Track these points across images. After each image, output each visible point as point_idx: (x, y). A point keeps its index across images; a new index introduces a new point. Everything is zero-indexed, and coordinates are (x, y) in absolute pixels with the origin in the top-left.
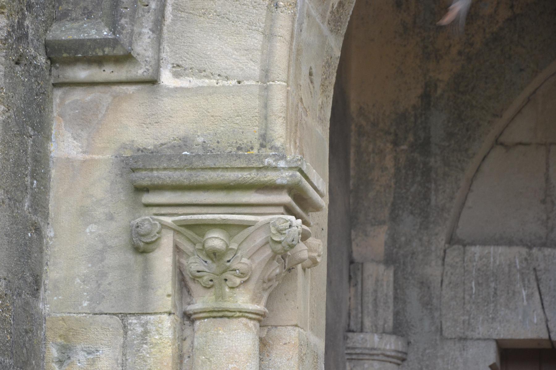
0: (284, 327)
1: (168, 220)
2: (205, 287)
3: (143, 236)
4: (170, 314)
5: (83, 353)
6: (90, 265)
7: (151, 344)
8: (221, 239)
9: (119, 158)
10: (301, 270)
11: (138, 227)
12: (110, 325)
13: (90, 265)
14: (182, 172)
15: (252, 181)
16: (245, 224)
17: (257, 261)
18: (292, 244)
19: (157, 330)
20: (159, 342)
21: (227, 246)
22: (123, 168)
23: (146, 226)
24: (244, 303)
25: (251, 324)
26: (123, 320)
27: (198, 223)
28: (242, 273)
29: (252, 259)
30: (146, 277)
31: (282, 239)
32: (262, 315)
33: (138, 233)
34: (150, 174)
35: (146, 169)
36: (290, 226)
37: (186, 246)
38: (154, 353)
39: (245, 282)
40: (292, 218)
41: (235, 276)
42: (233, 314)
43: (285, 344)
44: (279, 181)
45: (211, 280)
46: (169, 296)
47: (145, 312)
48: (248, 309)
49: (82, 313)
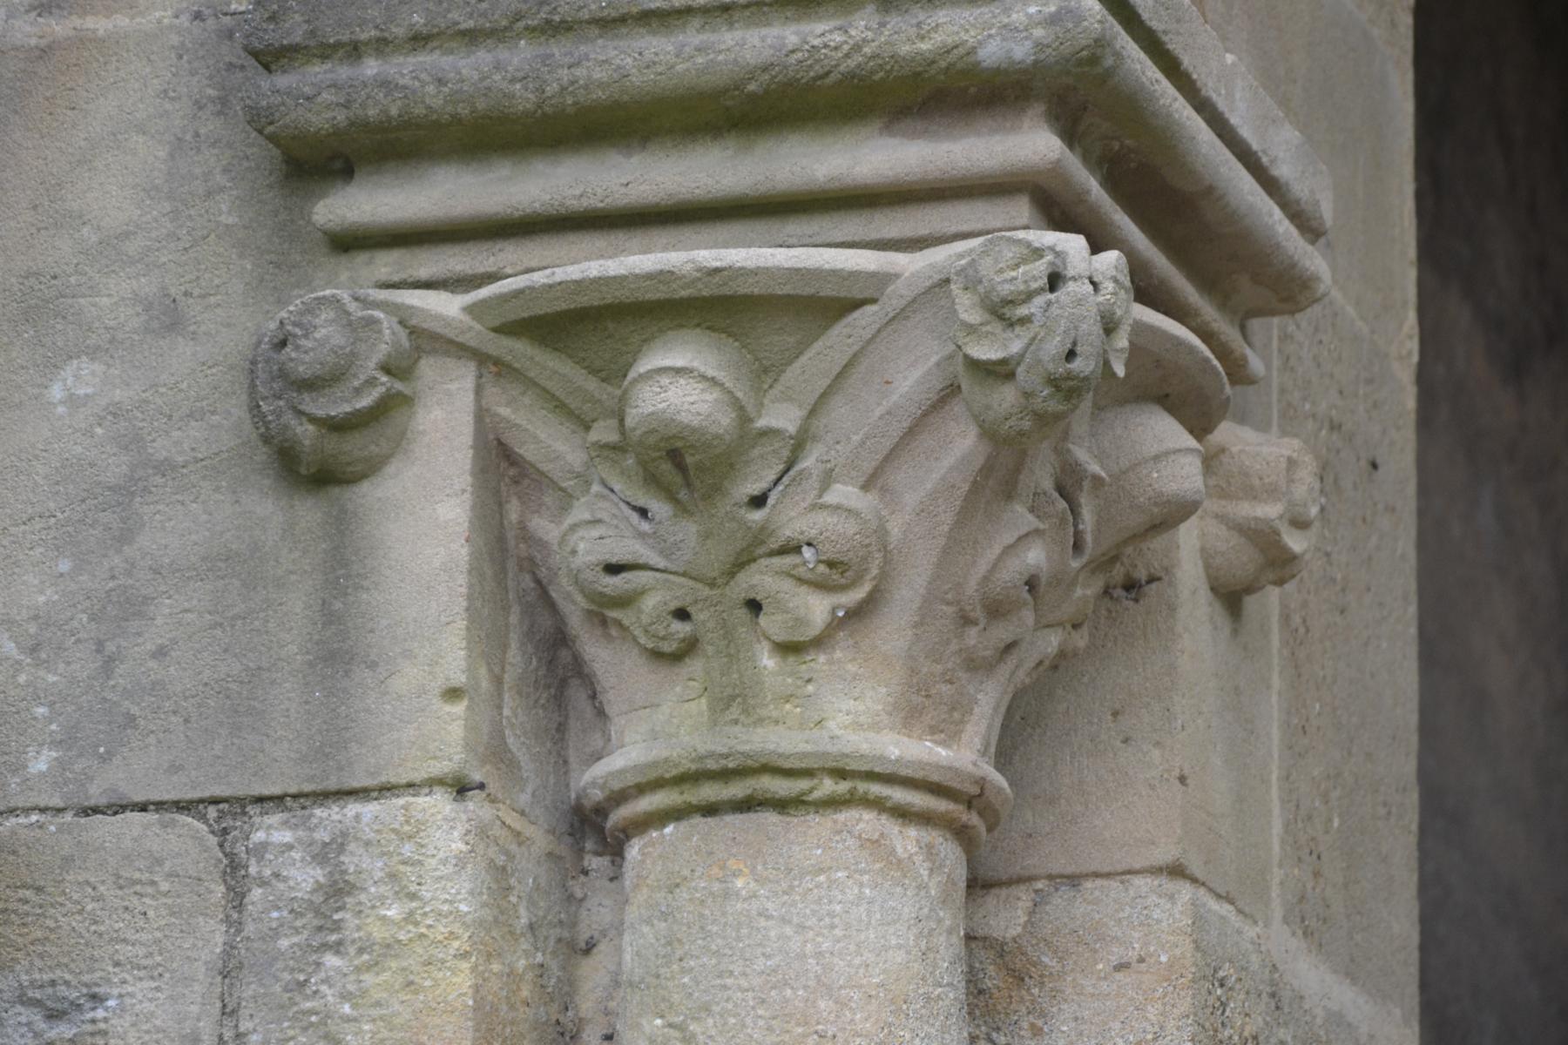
0: (1114, 884)
1: (447, 306)
2: (657, 655)
3: (310, 385)
4: (461, 788)
5: (26, 1014)
6: (64, 566)
7: (361, 951)
8: (704, 377)
9: (211, 22)
10: (1204, 594)
11: (283, 344)
12: (159, 862)
13: (64, 566)
14: (503, 54)
15: (851, 63)
16: (828, 291)
17: (911, 499)
18: (1069, 376)
19: (393, 876)
20: (402, 936)
21: (744, 419)
22: (231, 65)
23: (320, 333)
24: (858, 726)
25: (907, 840)
26: (225, 831)
27: (583, 301)
28: (831, 564)
29: (884, 490)
30: (338, 605)
31: (1015, 347)
32: (969, 802)
33: (283, 374)
34: (344, 72)
35: (326, 52)
36: (1055, 281)
37: (548, 442)
38: (377, 995)
39: (857, 614)
40: (1073, 244)
41: (801, 581)
42: (802, 784)
43: (1121, 967)
44: (992, 52)
45: (682, 614)
46: (453, 694)
47: (332, 784)
48: (882, 758)
49: (27, 811)
